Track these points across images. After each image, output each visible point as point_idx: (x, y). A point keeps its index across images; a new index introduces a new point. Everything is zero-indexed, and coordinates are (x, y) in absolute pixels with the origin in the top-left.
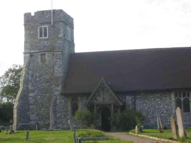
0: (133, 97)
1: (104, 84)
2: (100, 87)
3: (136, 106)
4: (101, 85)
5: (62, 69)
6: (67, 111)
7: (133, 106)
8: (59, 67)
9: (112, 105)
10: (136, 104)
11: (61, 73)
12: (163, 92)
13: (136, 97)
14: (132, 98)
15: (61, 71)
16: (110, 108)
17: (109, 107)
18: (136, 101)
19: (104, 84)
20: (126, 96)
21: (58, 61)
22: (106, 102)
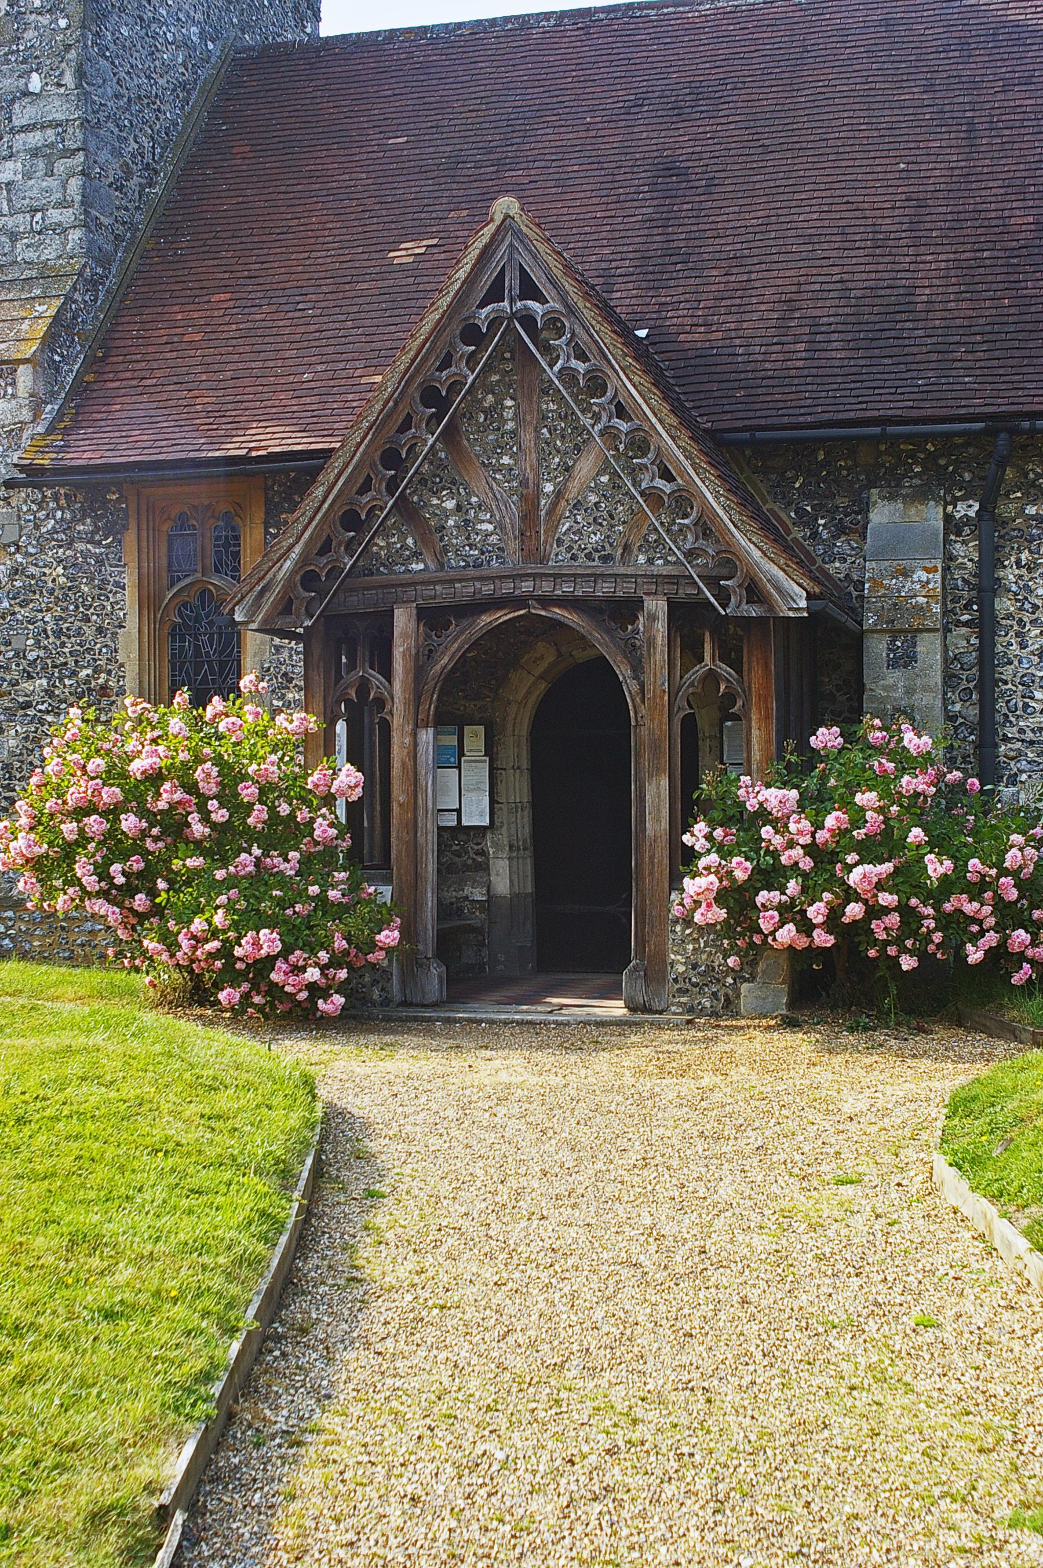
0: (968, 509)
1: (529, 290)
2: (472, 334)
3: (1007, 643)
4: (495, 293)
5: (75, 184)
6: (104, 689)
7: (963, 640)
8: (35, 153)
9: (657, 606)
10: (1004, 605)
11: (60, 230)
12: (997, 548)
13: (1007, 509)
14: (948, 518)
15: (63, 204)
16: (623, 671)
17: (602, 642)
18: (1010, 575)
19: (529, 290)
20: (865, 509)
21: (35, 83)
22: (558, 557)
